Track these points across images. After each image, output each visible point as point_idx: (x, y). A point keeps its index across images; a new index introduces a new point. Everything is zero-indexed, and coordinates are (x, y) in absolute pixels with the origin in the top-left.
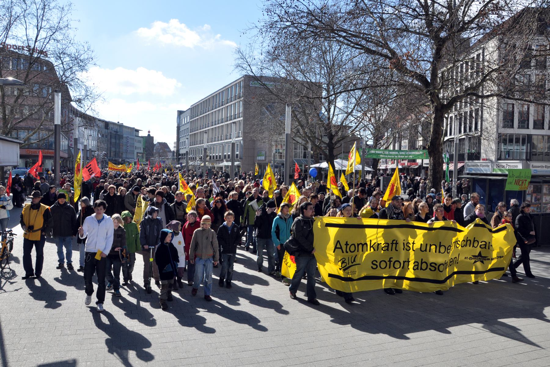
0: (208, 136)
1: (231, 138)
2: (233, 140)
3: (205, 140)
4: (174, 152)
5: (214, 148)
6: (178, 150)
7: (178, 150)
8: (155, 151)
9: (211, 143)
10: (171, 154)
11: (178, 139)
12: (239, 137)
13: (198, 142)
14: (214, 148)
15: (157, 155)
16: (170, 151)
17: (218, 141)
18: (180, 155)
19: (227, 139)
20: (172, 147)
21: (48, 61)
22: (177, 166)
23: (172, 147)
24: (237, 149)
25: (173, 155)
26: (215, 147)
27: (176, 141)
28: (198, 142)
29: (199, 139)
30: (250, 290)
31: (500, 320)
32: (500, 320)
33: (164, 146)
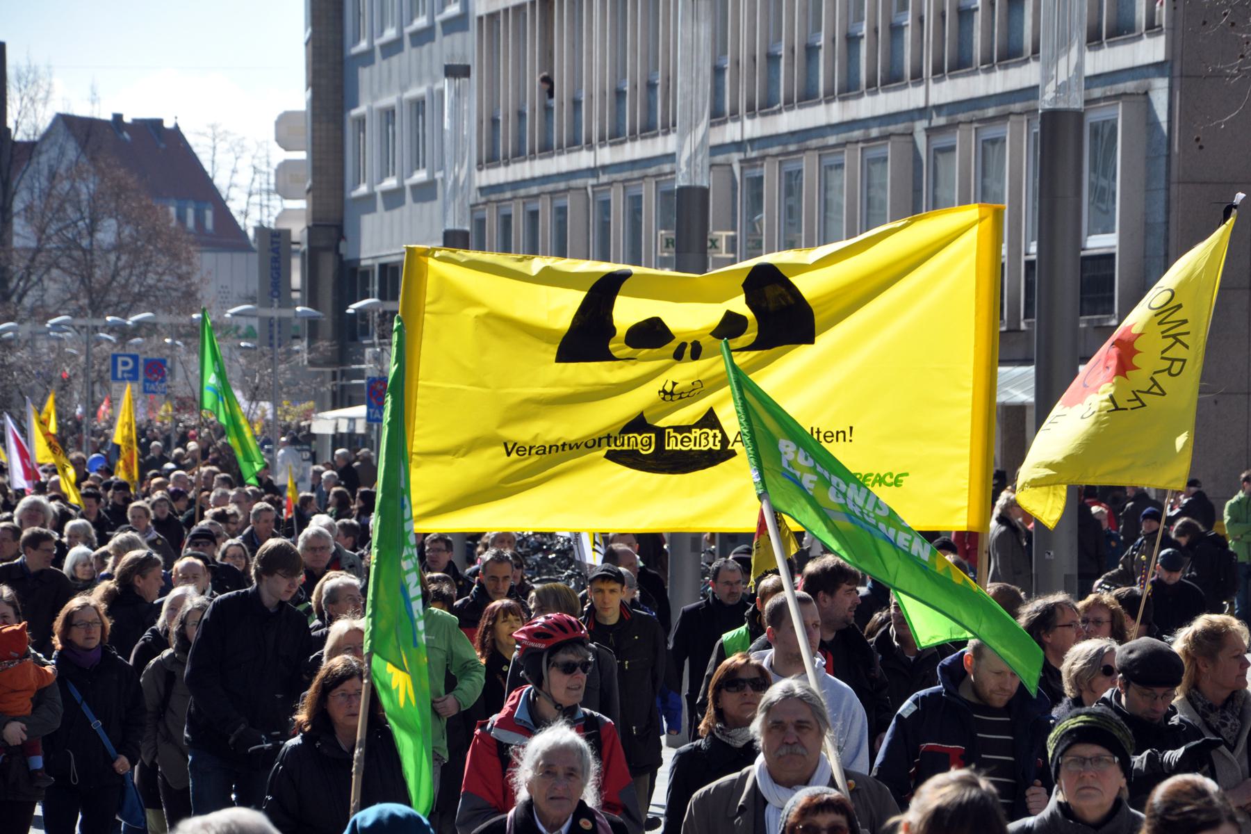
0: (720, 42)
1: (1010, 54)
2: (1058, 73)
3: (690, 85)
4: (274, 240)
5: (791, 184)
6: (332, 225)
7: (332, 225)
8: (22, 234)
9: (753, 128)
10: (244, 272)
11: (332, 67)
12: (1122, 30)
13: (595, 119)
14: (791, 184)
15: (53, 287)
16: (226, 233)
17: (849, 89)
18: (351, 279)
19: (962, 64)
20: (248, 152)
21: (587, 781)
22: (326, 423)
23: (248, 152)
24: (1103, 196)
25: (276, 286)
26: (809, 165)
27: (295, 95)
28: (595, 119)
29: (596, 76)
30: (224, 511)
31: (687, 662)
32: (687, 662)
33: (150, 159)
